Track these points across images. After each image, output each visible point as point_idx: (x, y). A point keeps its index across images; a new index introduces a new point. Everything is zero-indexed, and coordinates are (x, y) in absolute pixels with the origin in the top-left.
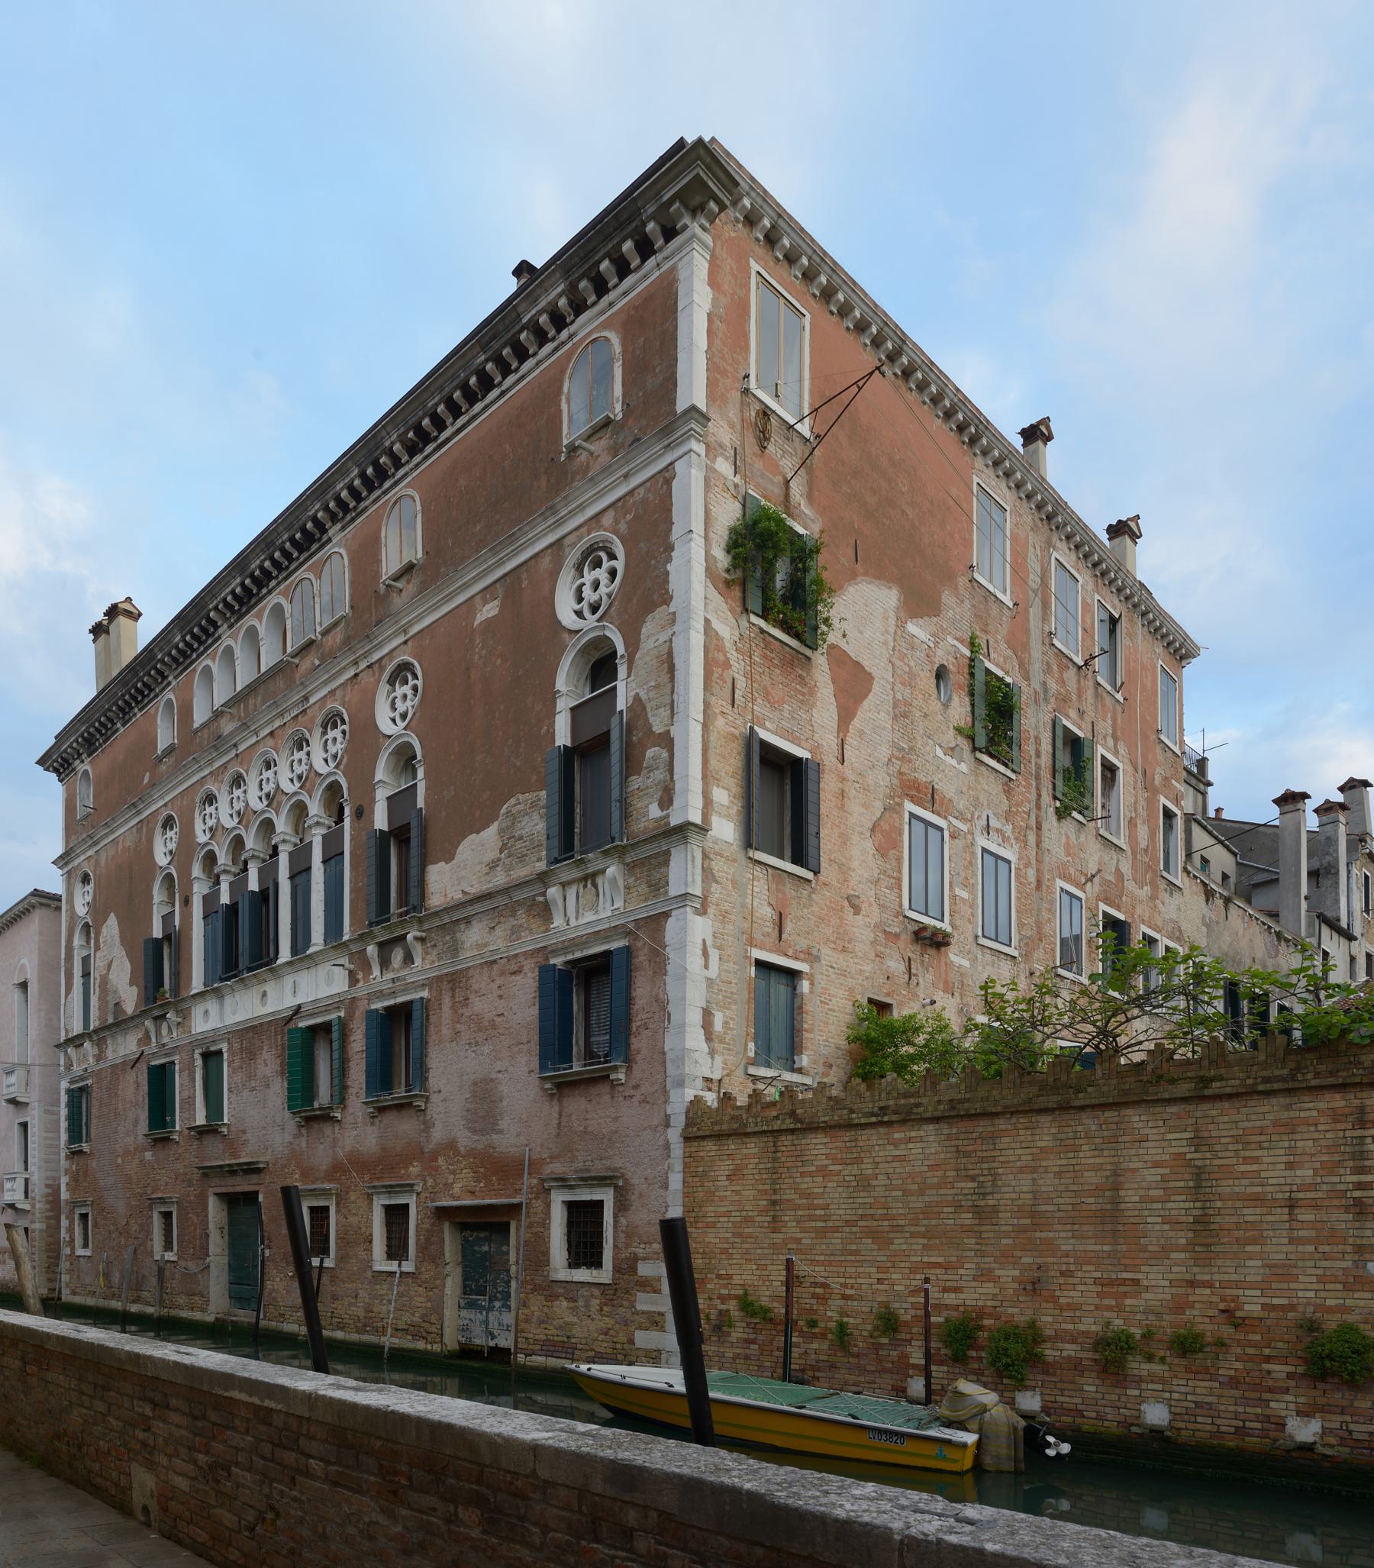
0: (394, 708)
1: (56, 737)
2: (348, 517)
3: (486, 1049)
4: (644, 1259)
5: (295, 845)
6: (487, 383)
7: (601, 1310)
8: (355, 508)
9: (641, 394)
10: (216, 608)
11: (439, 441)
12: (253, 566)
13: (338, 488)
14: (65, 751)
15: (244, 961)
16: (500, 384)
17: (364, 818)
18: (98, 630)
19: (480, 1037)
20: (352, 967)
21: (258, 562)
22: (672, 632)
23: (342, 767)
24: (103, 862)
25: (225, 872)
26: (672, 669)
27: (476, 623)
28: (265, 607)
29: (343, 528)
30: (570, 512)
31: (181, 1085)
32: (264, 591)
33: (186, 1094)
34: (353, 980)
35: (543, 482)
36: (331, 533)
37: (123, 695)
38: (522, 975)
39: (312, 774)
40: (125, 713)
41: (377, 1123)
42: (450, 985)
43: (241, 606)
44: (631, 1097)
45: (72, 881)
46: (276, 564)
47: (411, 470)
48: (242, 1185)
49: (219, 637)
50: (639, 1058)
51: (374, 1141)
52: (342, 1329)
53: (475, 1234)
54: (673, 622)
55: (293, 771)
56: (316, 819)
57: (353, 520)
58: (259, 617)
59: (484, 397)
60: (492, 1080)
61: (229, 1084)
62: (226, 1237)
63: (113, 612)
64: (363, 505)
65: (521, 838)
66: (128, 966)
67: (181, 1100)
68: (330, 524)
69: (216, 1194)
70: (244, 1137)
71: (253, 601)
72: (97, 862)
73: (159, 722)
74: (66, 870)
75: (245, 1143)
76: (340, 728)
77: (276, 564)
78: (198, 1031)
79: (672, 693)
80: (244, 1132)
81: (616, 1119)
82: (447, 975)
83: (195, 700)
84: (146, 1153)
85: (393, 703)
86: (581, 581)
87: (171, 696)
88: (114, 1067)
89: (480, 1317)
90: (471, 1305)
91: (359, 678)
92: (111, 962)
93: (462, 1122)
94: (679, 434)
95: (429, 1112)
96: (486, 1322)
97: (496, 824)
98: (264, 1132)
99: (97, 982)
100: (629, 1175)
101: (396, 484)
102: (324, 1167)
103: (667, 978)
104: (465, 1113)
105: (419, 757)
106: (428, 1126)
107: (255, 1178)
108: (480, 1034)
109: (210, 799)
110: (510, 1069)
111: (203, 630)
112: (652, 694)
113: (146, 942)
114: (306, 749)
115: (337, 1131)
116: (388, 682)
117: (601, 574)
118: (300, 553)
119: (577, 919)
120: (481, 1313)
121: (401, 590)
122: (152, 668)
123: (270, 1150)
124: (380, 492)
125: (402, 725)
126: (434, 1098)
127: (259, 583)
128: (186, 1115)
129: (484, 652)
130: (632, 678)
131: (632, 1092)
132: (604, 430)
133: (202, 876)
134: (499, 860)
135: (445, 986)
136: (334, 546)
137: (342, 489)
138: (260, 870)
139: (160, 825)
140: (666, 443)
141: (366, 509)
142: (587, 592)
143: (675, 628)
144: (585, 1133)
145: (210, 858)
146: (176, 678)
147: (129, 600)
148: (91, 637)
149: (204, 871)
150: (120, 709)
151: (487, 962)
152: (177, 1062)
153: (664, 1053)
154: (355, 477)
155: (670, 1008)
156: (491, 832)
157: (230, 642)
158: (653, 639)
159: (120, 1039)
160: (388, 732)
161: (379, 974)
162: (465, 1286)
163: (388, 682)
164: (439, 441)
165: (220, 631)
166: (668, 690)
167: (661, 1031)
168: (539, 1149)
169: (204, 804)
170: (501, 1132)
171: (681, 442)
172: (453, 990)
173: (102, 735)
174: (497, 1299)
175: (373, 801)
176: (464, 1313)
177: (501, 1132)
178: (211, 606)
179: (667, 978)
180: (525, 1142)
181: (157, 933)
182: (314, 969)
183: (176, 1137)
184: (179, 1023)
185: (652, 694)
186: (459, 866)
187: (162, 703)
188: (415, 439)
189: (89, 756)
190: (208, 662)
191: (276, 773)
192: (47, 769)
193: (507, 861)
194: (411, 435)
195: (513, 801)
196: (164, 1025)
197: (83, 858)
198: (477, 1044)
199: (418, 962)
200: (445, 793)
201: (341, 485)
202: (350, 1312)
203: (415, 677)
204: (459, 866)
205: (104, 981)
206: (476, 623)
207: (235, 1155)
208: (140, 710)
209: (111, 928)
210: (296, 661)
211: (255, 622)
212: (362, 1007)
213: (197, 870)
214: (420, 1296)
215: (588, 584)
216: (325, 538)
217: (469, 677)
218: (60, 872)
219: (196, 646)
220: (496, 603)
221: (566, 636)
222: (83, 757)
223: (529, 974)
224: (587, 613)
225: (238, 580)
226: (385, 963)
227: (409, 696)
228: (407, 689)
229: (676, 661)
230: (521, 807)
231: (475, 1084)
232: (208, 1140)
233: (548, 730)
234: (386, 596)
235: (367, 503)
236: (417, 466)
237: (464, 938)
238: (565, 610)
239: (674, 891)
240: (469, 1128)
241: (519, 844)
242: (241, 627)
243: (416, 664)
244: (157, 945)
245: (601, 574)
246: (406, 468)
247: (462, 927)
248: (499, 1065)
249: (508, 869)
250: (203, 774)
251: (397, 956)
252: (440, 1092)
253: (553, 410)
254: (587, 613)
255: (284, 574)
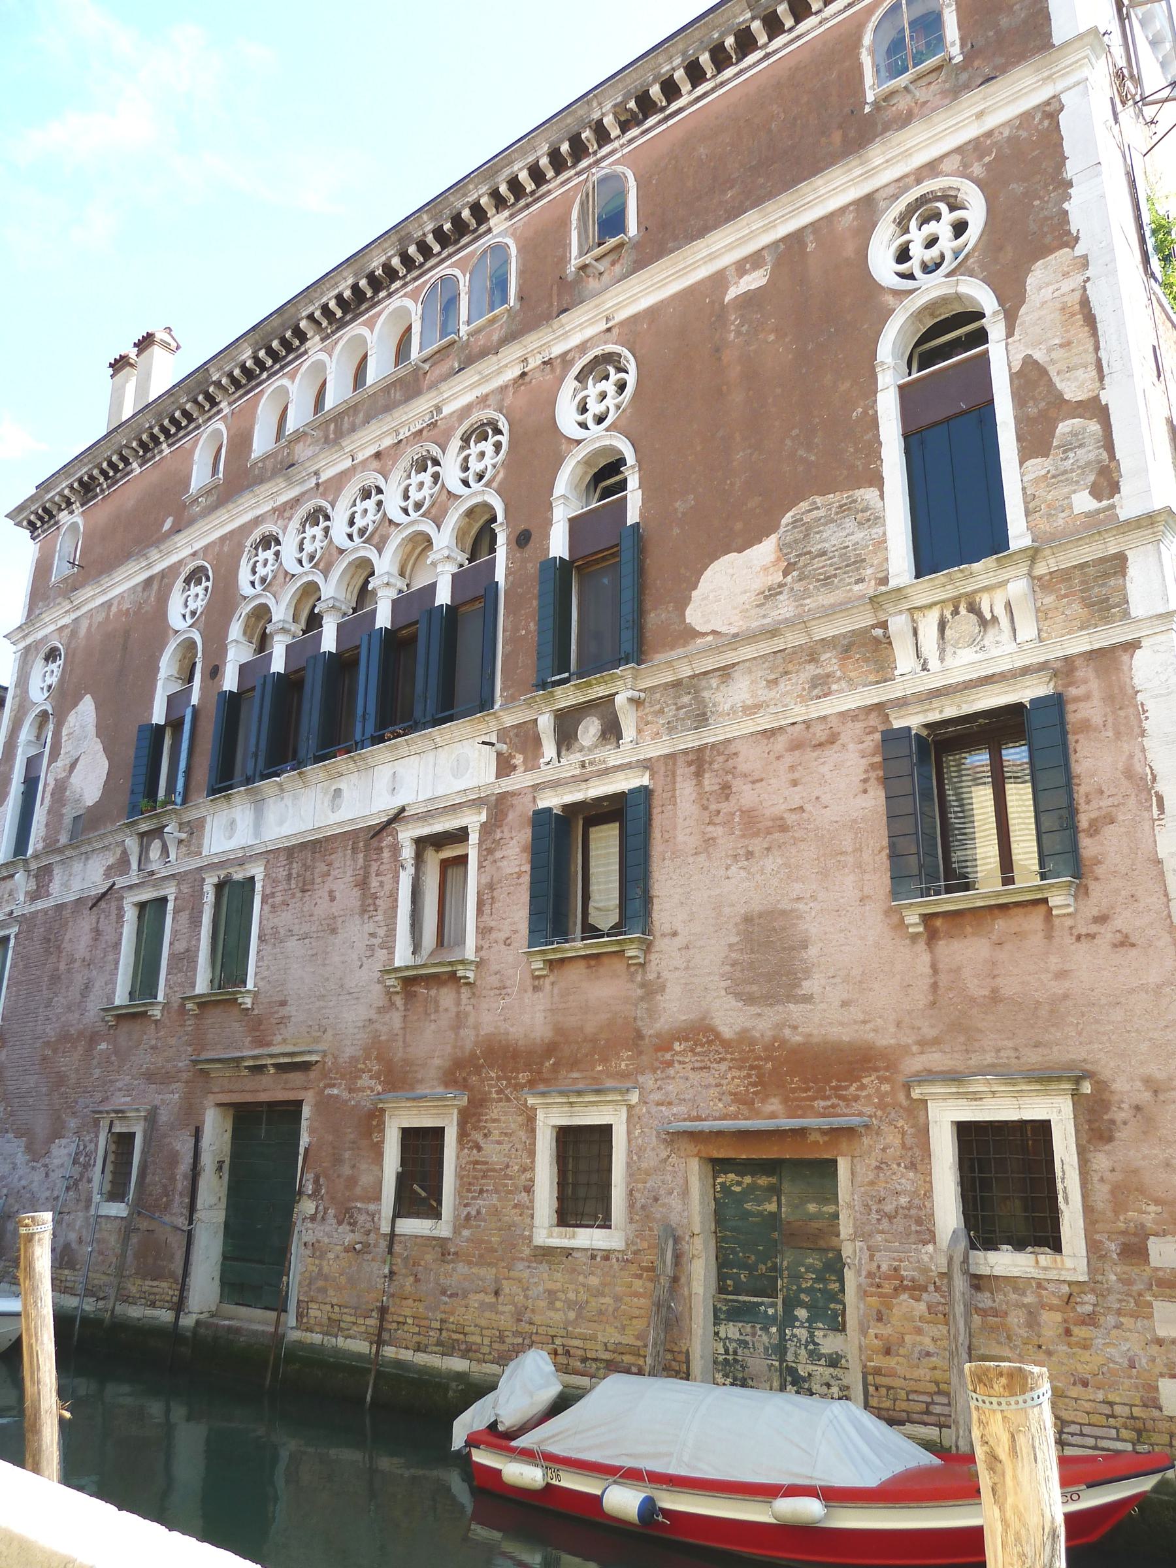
0: (254, 572)
1: (37, 488)
2: (522, 203)
3: (771, 863)
4: (1156, 1235)
5: (401, 591)
6: (746, 43)
7: (1068, 1332)
8: (533, 193)
9: (991, 34)
10: (311, 317)
11: (668, 112)
12: (375, 264)
13: (516, 168)
14: (51, 500)
15: (244, 760)
16: (765, 45)
17: (531, 544)
18: (120, 364)
19: (757, 844)
20: (504, 748)
21: (383, 259)
22: (1084, 278)
23: (495, 485)
24: (83, 631)
25: (284, 630)
26: (1091, 321)
27: (727, 299)
28: (379, 314)
29: (512, 216)
30: (887, 161)
31: (175, 933)
32: (382, 294)
33: (181, 946)
34: (504, 767)
35: (837, 137)
36: (492, 222)
37: (151, 428)
38: (836, 747)
39: (444, 496)
40: (86, 492)
41: (548, 987)
42: (693, 769)
43: (345, 313)
44: (1091, 936)
45: (30, 658)
46: (407, 261)
47: (622, 146)
48: (271, 1090)
49: (306, 352)
50: (1100, 871)
51: (539, 1017)
52: (466, 1354)
53: (748, 1180)
54: (1086, 265)
55: (187, 606)
56: (280, 625)
57: (528, 206)
58: (371, 325)
59: (739, 60)
60: (783, 913)
61: (261, 929)
62: (226, 1177)
63: (145, 343)
64: (544, 188)
65: (823, 553)
66: (103, 765)
67: (172, 956)
68: (494, 210)
69: (219, 1105)
70: (284, 1011)
71: (363, 307)
72: (74, 633)
73: (196, 457)
74: (22, 645)
75: (283, 1021)
76: (492, 439)
77: (407, 261)
78: (214, 851)
79: (1097, 348)
80: (283, 1004)
81: (1062, 975)
82: (686, 752)
83: (257, 427)
84: (1089, 1091)
85: (254, 566)
86: (408, 481)
87: (221, 426)
88: (60, 907)
89: (765, 1338)
90: (736, 1314)
91: (527, 379)
92: (77, 760)
93: (724, 984)
94: (1069, 62)
95: (652, 968)
96: (780, 1350)
97: (773, 538)
98: (322, 1003)
99: (49, 789)
100: (1105, 1074)
101: (597, 162)
102: (437, 1062)
103: (1146, 742)
104: (728, 968)
105: (500, 517)
106: (652, 990)
107: (296, 1077)
108: (757, 841)
109: (268, 541)
110: (822, 895)
111: (285, 343)
112: (1055, 355)
113: (142, 729)
114: (323, 524)
115: (464, 1000)
116: (577, 378)
117: (609, 386)
118: (443, 248)
119: (942, 659)
120: (765, 1329)
121: (601, 274)
122: (95, 467)
123: (330, 1032)
124: (573, 172)
125: (414, 515)
126: (661, 944)
127: (375, 283)
128: (180, 978)
129: (744, 329)
130: (1017, 337)
131: (1094, 929)
132: (934, 75)
133: (242, 639)
134: (781, 585)
135: (683, 770)
136: (495, 237)
137: (521, 169)
138: (340, 627)
139: (182, 577)
140: (1046, 74)
141: (549, 192)
142: (412, 492)
143: (1088, 273)
144: (995, 997)
145: (262, 613)
146: (230, 404)
147: (168, 330)
148: (111, 371)
149: (245, 633)
150: (142, 444)
151: (764, 732)
152: (171, 898)
153: (1159, 862)
154: (543, 155)
155: (1160, 787)
156: (765, 550)
157: (323, 356)
158: (1051, 289)
159: (77, 867)
160: (244, 593)
161: (555, 755)
162: (721, 1277)
163: (577, 378)
164: (668, 112)
165: (308, 344)
166: (1090, 347)
167: (1147, 826)
168: (892, 1029)
169: (256, 549)
170: (808, 999)
171: (1068, 73)
172: (699, 774)
173: (107, 477)
174: (802, 1304)
175: (549, 523)
176: (731, 1330)
177: (808, 999)
178: (304, 314)
179: (1146, 742)
180: (861, 1017)
181: (158, 716)
182: (431, 754)
183: (156, 1012)
184: (181, 841)
185: (1055, 355)
186: (706, 598)
187: (345, 339)
188: (636, 109)
189: (82, 505)
190: (285, 382)
191: (277, 554)
192: (18, 524)
193: (797, 587)
194: (632, 104)
195: (804, 505)
196: (156, 845)
197: (52, 628)
198: (749, 855)
199: (629, 731)
200: (677, 504)
201: (521, 165)
202: (483, 1323)
203: (208, 579)
204: (706, 598)
205: (61, 787)
206: (727, 299)
207: (261, 1042)
208: (169, 446)
209: (86, 712)
210: (426, 366)
211: (364, 331)
212: (524, 808)
213: (236, 630)
214: (636, 1295)
215: (359, 512)
216: (483, 228)
217: (719, 359)
218: (14, 648)
219: (269, 362)
220: (761, 271)
221: (890, 299)
222: (74, 506)
223: (851, 746)
224: (355, 537)
225: (350, 281)
226: (566, 736)
227: (201, 596)
228: (200, 590)
229: (1097, 310)
230: (821, 513)
231: (748, 919)
232: (214, 1017)
233: (865, 413)
234: (578, 281)
235: (551, 186)
236: (630, 141)
237: (718, 697)
238: (567, 419)
239: (1138, 608)
240: (738, 995)
241: (818, 563)
242: (340, 337)
243: (625, 352)
244: (159, 730)
245: (609, 386)
246: (616, 144)
247: (714, 682)
248: (797, 888)
249: (799, 597)
250: (259, 512)
251: (590, 729)
252: (675, 934)
253: (847, 64)
254: (590, 423)
255: (415, 273)
